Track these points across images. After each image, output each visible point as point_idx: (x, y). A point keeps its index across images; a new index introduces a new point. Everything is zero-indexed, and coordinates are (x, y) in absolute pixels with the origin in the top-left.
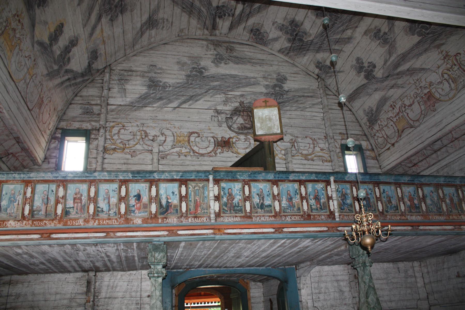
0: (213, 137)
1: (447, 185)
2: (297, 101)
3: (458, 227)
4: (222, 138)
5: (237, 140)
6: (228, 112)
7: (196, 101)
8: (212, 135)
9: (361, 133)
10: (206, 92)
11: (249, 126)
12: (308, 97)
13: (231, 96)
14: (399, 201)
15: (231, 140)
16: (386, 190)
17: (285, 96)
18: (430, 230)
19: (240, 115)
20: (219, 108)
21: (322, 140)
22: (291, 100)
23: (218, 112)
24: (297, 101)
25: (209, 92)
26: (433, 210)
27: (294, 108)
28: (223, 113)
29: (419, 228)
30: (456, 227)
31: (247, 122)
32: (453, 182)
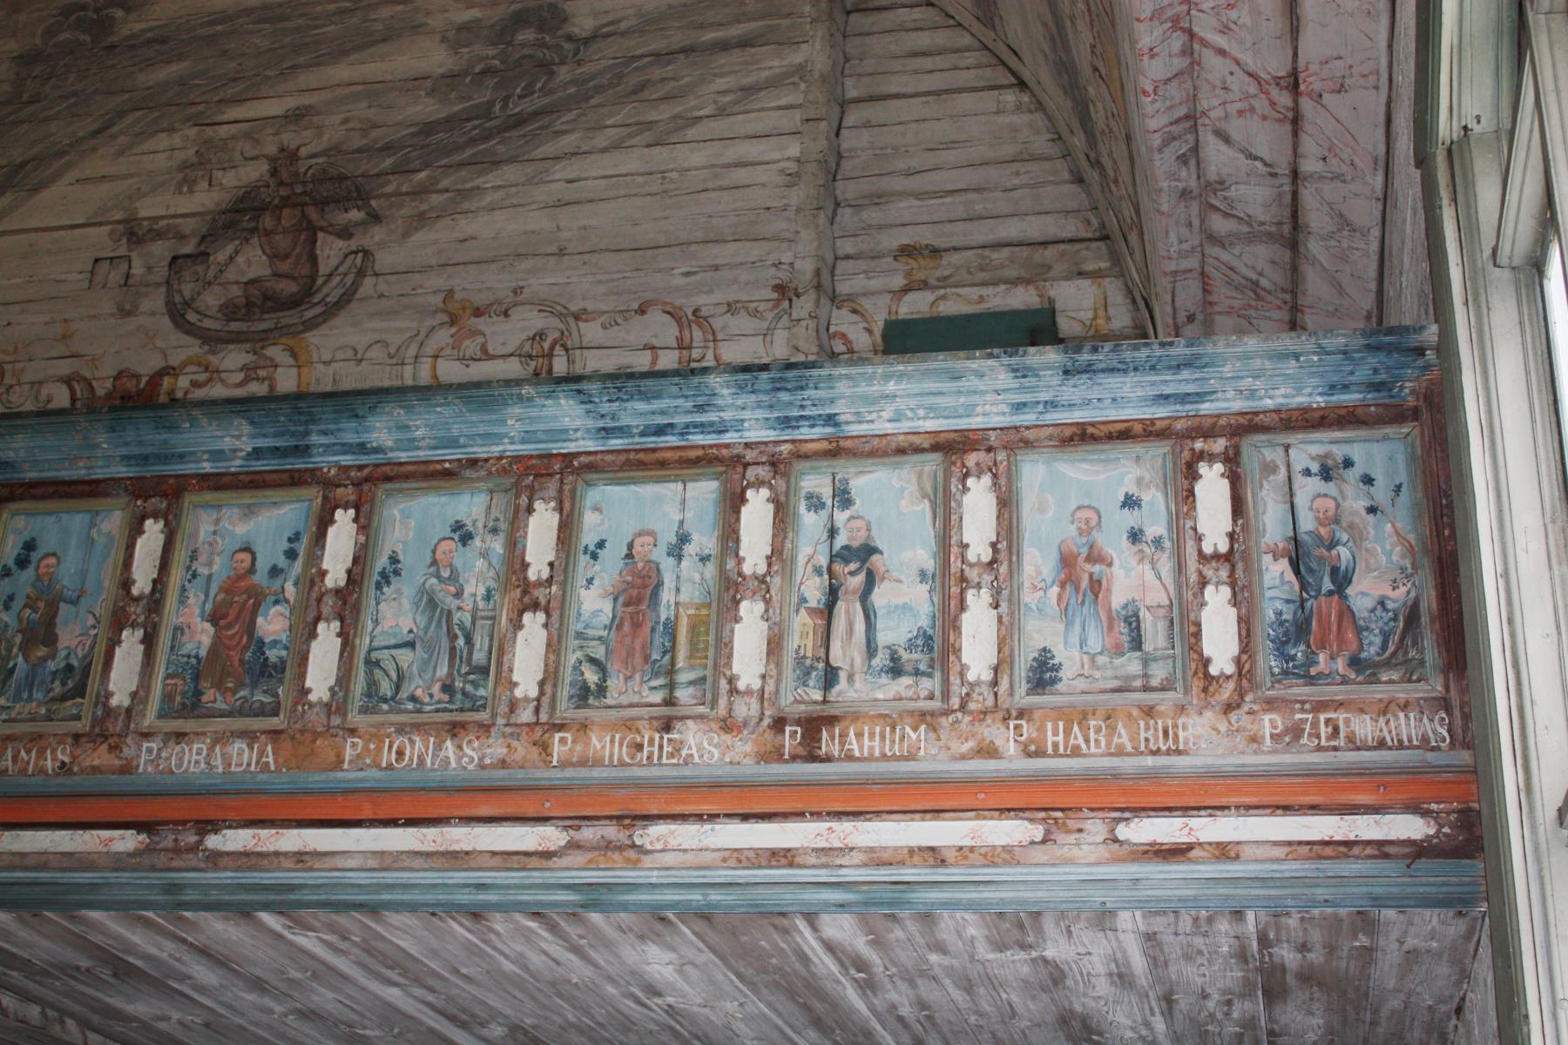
0: (68, 381)
1: (641, 465)
2: (643, 86)
3: (611, 831)
4: (118, 377)
5: (202, 377)
6: (188, 226)
7: (36, 190)
8: (65, 368)
9: (1071, 228)
10: (98, 132)
11: (291, 288)
12: (724, 46)
13: (234, 128)
14: (119, 622)
15: (167, 382)
16: (48, 543)
17: (564, 73)
18: (300, 857)
19: (253, 231)
20: (148, 209)
21: (755, 314)
22: (599, 89)
23: (135, 233)
24: (643, 86)
25: (115, 129)
26: (416, 686)
27: (601, 140)
28: (159, 235)
29: (213, 842)
30: (589, 833)
31: (285, 267)
32: (702, 427)
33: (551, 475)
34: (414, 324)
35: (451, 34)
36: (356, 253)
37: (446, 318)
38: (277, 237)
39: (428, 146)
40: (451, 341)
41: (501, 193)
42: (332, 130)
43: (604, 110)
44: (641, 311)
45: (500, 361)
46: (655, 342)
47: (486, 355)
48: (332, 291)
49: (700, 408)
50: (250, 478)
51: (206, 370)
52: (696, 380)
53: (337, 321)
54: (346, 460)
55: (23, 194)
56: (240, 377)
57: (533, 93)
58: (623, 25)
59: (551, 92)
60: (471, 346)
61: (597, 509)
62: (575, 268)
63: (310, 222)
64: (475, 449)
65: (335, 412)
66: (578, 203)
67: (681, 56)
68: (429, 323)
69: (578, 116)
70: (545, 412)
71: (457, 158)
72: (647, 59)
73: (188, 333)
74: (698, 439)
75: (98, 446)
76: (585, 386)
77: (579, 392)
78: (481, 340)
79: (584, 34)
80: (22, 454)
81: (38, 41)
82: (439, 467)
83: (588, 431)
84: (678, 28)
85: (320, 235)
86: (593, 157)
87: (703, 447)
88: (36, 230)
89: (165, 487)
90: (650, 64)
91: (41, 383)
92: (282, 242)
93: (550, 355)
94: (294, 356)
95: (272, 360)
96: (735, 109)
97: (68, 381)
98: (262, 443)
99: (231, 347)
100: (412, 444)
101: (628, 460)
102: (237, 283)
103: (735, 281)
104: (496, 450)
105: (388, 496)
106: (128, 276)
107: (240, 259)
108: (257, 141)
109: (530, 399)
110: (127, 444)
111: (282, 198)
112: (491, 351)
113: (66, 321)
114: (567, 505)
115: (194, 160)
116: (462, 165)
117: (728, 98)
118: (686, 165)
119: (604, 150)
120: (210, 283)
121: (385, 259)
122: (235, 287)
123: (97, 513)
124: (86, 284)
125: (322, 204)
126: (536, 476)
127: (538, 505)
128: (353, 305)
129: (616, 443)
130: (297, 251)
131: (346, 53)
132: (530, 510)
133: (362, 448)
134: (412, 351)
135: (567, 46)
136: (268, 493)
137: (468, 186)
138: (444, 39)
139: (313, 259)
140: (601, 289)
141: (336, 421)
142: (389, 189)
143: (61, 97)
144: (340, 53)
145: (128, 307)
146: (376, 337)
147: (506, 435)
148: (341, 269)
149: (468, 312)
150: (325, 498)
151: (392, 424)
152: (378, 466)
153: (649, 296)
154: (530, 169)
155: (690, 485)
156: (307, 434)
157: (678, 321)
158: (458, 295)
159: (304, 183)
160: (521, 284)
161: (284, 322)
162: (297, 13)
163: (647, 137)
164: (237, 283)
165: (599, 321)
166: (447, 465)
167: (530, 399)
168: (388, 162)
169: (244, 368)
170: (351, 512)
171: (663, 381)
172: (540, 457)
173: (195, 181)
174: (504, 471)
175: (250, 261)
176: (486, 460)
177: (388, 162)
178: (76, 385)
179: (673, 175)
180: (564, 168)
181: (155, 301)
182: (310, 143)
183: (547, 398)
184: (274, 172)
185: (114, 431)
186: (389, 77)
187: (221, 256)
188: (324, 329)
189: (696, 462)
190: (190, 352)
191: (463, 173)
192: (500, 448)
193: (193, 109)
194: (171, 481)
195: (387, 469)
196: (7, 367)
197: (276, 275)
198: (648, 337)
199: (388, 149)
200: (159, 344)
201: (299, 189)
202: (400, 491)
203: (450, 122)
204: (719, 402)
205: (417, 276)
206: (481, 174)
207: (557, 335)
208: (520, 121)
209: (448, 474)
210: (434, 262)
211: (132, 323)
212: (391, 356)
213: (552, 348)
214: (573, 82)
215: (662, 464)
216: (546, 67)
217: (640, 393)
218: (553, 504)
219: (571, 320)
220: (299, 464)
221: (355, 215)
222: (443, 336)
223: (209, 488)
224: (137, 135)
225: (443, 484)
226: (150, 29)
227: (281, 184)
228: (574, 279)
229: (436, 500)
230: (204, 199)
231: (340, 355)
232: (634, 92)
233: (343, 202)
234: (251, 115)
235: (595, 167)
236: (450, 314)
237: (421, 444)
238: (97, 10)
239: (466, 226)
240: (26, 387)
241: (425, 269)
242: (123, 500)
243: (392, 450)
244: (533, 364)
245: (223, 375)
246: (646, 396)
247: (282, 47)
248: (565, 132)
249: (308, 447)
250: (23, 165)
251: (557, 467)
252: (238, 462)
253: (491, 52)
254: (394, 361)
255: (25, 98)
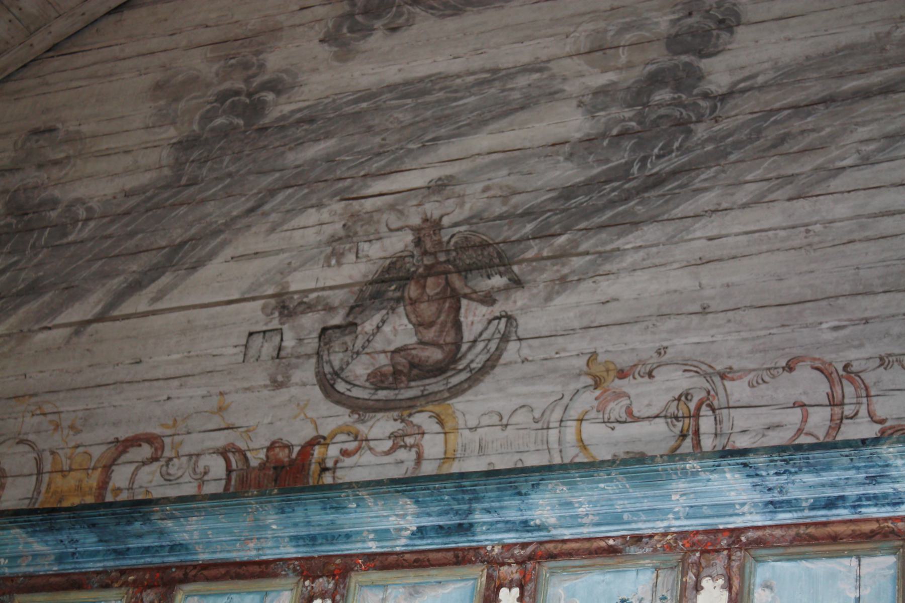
0: (223, 453)
1: (812, 540)
2: (782, 140)
4: (270, 448)
5: (352, 446)
6: (336, 297)
7: (194, 268)
8: (221, 440)
10: (252, 210)
11: (435, 355)
12: (865, 94)
13: (379, 201)
15: (317, 451)
17: (701, 131)
19: (399, 300)
20: (298, 282)
22: (738, 145)
23: (286, 306)
24: (782, 140)
25: (267, 207)
27: (742, 195)
28: (310, 307)
32: (876, 500)
33: (718, 551)
34: (559, 388)
35: (587, 99)
36: (499, 318)
37: (589, 381)
38: (423, 306)
39: (567, 209)
40: (596, 403)
41: (642, 254)
42: (474, 198)
43: (742, 166)
44: (789, 368)
45: (646, 423)
46: (805, 400)
47: (631, 417)
48: (476, 357)
49: (873, 480)
50: (415, 557)
51: (356, 439)
52: (868, 451)
53: (482, 387)
54: (510, 538)
55: (183, 272)
56: (389, 444)
57: (672, 151)
58: (760, 80)
59: (689, 150)
60: (616, 409)
61: (767, 586)
62: (719, 326)
63: (454, 290)
64: (640, 525)
65: (499, 489)
66: (720, 260)
67: (821, 107)
68: (573, 386)
69: (717, 173)
70: (711, 486)
71: (597, 220)
72: (786, 112)
73: (338, 403)
74: (872, 512)
75: (267, 527)
76: (751, 459)
77: (745, 465)
78: (625, 402)
79: (720, 91)
80: (196, 536)
81: (195, 127)
82: (602, 544)
83: (755, 505)
84: (817, 79)
85: (464, 302)
86: (733, 213)
87: (877, 520)
88: (194, 307)
89: (332, 567)
90: (789, 117)
91: (198, 455)
92: (427, 310)
93: (697, 416)
94: (441, 423)
95: (419, 427)
96: (880, 157)
97: (223, 453)
98: (426, 522)
99: (379, 415)
100: (575, 521)
101: (798, 535)
102: (384, 352)
103: (887, 334)
104: (660, 526)
105: (552, 574)
106: (280, 349)
107: (387, 329)
108: (401, 212)
109: (695, 474)
110: (296, 525)
111: (427, 267)
112: (636, 413)
113: (221, 394)
114: (736, 583)
115: (342, 233)
116: (602, 227)
117: (872, 146)
118: (830, 217)
119: (744, 206)
120: (358, 353)
121: (527, 324)
122: (382, 356)
123: (267, 594)
124: (241, 358)
125: (465, 271)
126: (703, 552)
127: (706, 583)
128: (497, 370)
129: (785, 517)
130: (442, 318)
131: (484, 123)
132: (698, 588)
133: (525, 526)
134: (557, 415)
135: (703, 103)
136: (433, 572)
137: (609, 247)
138: (580, 104)
139: (458, 326)
140: (747, 347)
141: (499, 499)
142: (530, 254)
143: (216, 178)
144: (479, 125)
145: (280, 378)
146: (521, 401)
147: (670, 510)
148: (485, 336)
149: (612, 374)
150: (490, 577)
151: (555, 501)
152: (541, 543)
153: (797, 352)
154: (670, 228)
155: (865, 561)
156: (470, 512)
157: (828, 376)
158: (601, 358)
159: (448, 252)
160: (665, 344)
161: (431, 389)
162: (437, 87)
163: (789, 190)
164: (384, 352)
165: (746, 380)
166: (611, 542)
167: (695, 474)
168: (529, 227)
169: (393, 436)
170: (516, 591)
171: (833, 453)
172: (706, 532)
173: (342, 254)
174: (669, 548)
175: (397, 331)
176: (651, 536)
177: (529, 227)
178: (231, 456)
179: (818, 228)
180: (705, 226)
181: (306, 372)
182: (452, 212)
183: (712, 472)
184: (418, 242)
185: (283, 512)
186: (528, 145)
187: (369, 326)
188: (469, 396)
189: (870, 536)
190: (340, 421)
191: (604, 235)
192: (665, 524)
193: (340, 185)
194: (338, 561)
195: (550, 546)
196: (167, 441)
197: (421, 342)
198: (796, 394)
199: (528, 214)
200: (310, 414)
201: (442, 258)
202: (564, 569)
203: (590, 185)
204: (893, 473)
205: (560, 340)
206: (620, 235)
207: (703, 394)
208: (658, 181)
209: (612, 551)
210: (576, 324)
211: (284, 395)
212: (536, 421)
213: (698, 408)
214: (710, 140)
215: (834, 539)
216: (683, 126)
217: (809, 465)
218: (721, 582)
219: (717, 379)
220: (463, 542)
221: (498, 281)
222: (588, 399)
223: (376, 568)
224: (288, 211)
225: (610, 561)
226: (300, 110)
227: (425, 253)
228: (719, 338)
229: (601, 577)
230: (353, 271)
231: (485, 421)
232: (774, 146)
233: (486, 268)
234: (394, 187)
235: (735, 223)
236: (595, 377)
237: (585, 521)
238: (250, 95)
239: (607, 288)
240: (184, 460)
241: (569, 332)
242: (292, 580)
243: (555, 527)
244: (680, 425)
245: (372, 444)
246: (815, 469)
247: (424, 120)
248: (706, 190)
249: (471, 525)
250: (183, 243)
251: (724, 543)
252: (403, 541)
253: (628, 113)
254: (539, 425)
255: (184, 181)
